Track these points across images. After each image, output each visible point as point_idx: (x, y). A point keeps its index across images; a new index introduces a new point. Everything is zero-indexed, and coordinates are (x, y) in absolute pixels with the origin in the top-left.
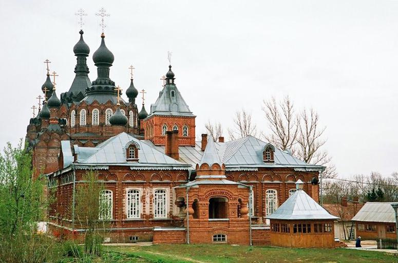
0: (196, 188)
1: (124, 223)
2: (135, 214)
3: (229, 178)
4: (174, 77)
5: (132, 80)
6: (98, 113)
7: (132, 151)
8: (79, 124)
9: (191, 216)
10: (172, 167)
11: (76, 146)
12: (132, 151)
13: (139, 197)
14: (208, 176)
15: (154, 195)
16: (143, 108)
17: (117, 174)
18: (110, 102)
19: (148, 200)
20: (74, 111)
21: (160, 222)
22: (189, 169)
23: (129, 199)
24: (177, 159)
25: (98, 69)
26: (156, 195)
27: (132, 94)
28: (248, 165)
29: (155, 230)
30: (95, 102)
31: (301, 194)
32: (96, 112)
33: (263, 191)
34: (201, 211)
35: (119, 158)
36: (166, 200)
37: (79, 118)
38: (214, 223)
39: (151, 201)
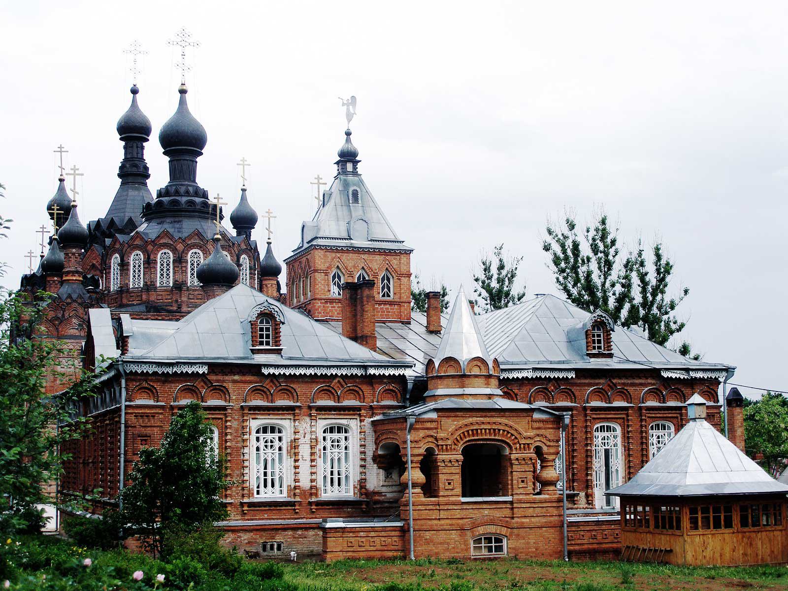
0: (431, 421)
1: (246, 508)
2: (273, 486)
3: (507, 395)
4: (358, 158)
5: (244, 190)
6: (171, 260)
7: (266, 329)
8: (127, 285)
9: (418, 490)
10: (365, 368)
11: (125, 318)
12: (266, 329)
13: (285, 445)
14: (459, 391)
15: (321, 439)
16: (269, 251)
17: (230, 386)
18: (198, 234)
19: (304, 451)
20: (117, 255)
21: (338, 507)
22: (408, 373)
23: (258, 449)
24: (374, 348)
25: (125, 148)
26: (324, 439)
27: (244, 222)
28: (551, 363)
29: (328, 525)
30: (166, 234)
31: (702, 431)
32: (164, 257)
33: (586, 427)
34: (442, 478)
35: (233, 347)
36: (350, 451)
37: (128, 270)
38: (471, 507)
39: (312, 454)
